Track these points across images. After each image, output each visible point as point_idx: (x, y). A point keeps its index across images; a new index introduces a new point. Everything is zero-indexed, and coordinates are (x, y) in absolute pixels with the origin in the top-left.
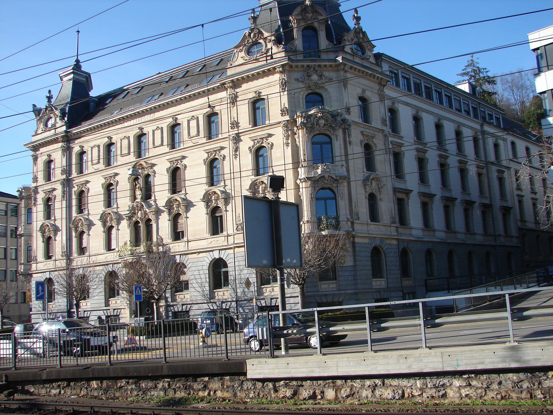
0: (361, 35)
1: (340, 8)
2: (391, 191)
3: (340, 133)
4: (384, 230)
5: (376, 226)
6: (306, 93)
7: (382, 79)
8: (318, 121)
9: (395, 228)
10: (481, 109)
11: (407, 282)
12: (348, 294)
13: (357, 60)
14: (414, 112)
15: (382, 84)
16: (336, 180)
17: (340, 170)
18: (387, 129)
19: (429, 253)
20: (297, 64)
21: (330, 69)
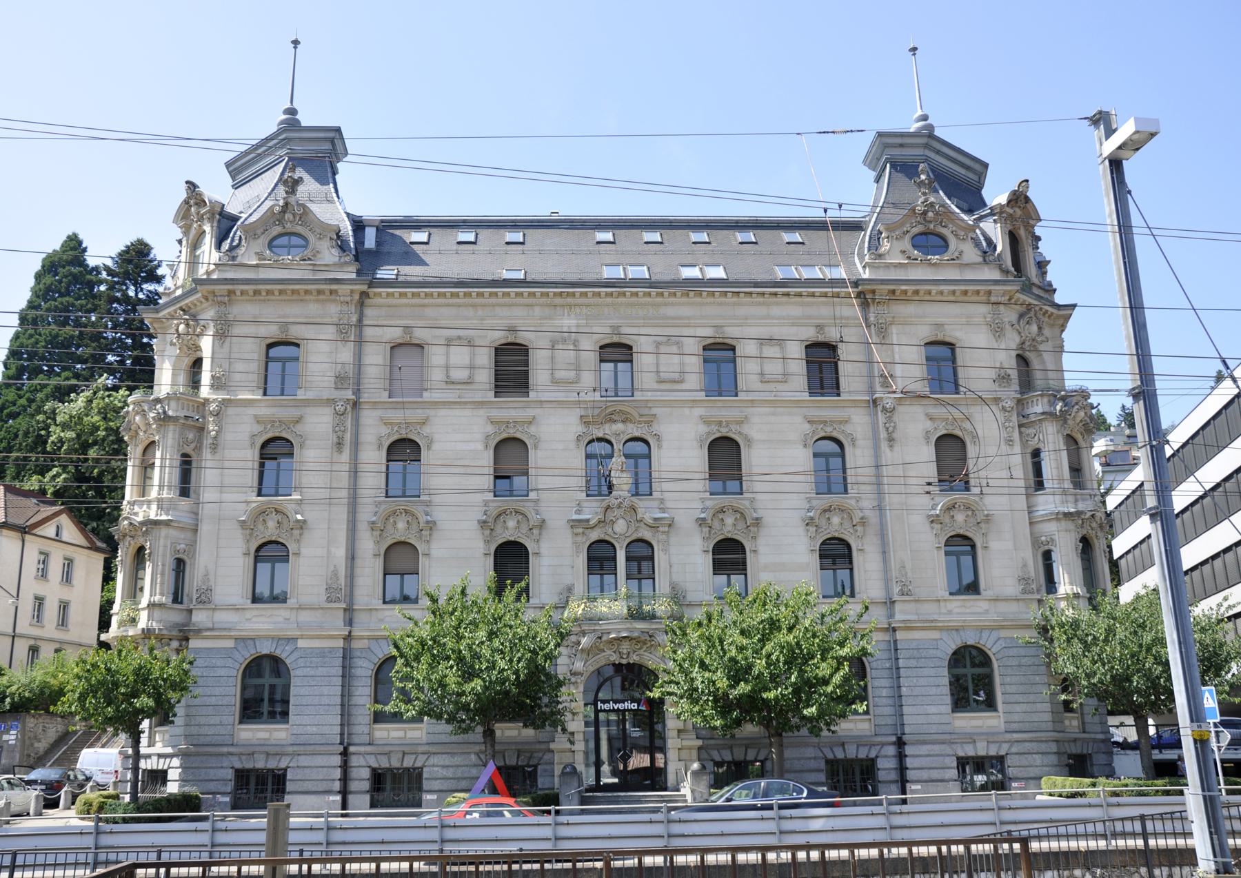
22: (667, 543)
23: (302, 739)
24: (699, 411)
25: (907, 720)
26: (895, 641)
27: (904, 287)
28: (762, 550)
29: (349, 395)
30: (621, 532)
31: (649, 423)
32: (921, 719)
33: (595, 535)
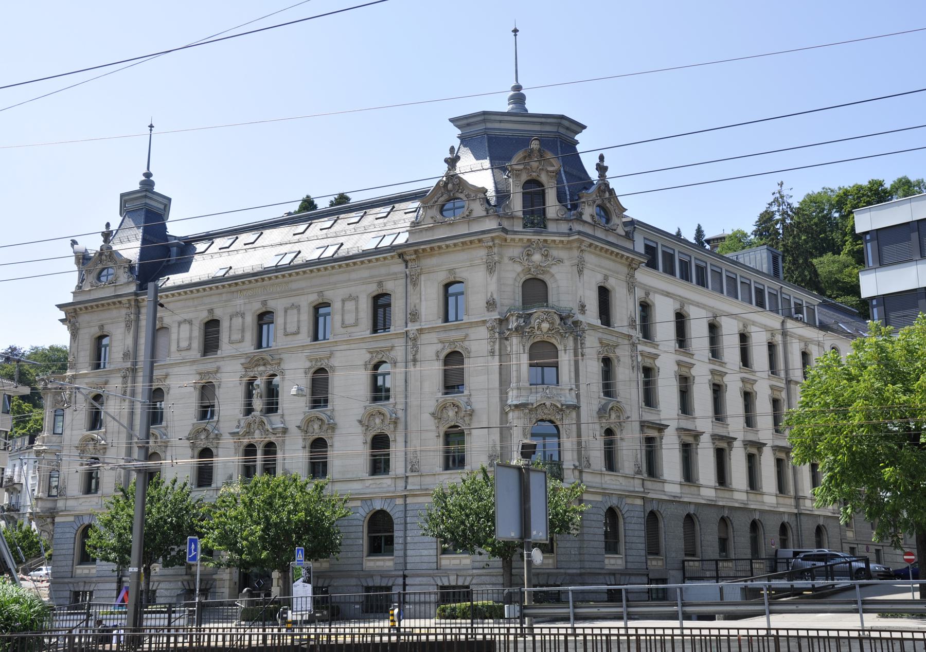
0: (607, 195)
1: (577, 147)
2: (637, 426)
3: (570, 342)
4: (624, 482)
5: (613, 478)
6: (524, 279)
7: (633, 259)
8: (540, 324)
9: (641, 481)
10: (784, 296)
11: (654, 563)
12: (569, 575)
13: (600, 234)
14: (678, 306)
15: (632, 266)
16: (561, 410)
17: (568, 395)
18: (637, 334)
19: (689, 519)
20: (513, 236)
21: (560, 245)
22: (284, 441)
23: (101, 573)
24: (307, 352)
25: (409, 560)
26: (406, 505)
27: (423, 247)
28: (336, 444)
29: (129, 365)
30: (258, 438)
31: (279, 364)
32: (417, 559)
33: (246, 441)
